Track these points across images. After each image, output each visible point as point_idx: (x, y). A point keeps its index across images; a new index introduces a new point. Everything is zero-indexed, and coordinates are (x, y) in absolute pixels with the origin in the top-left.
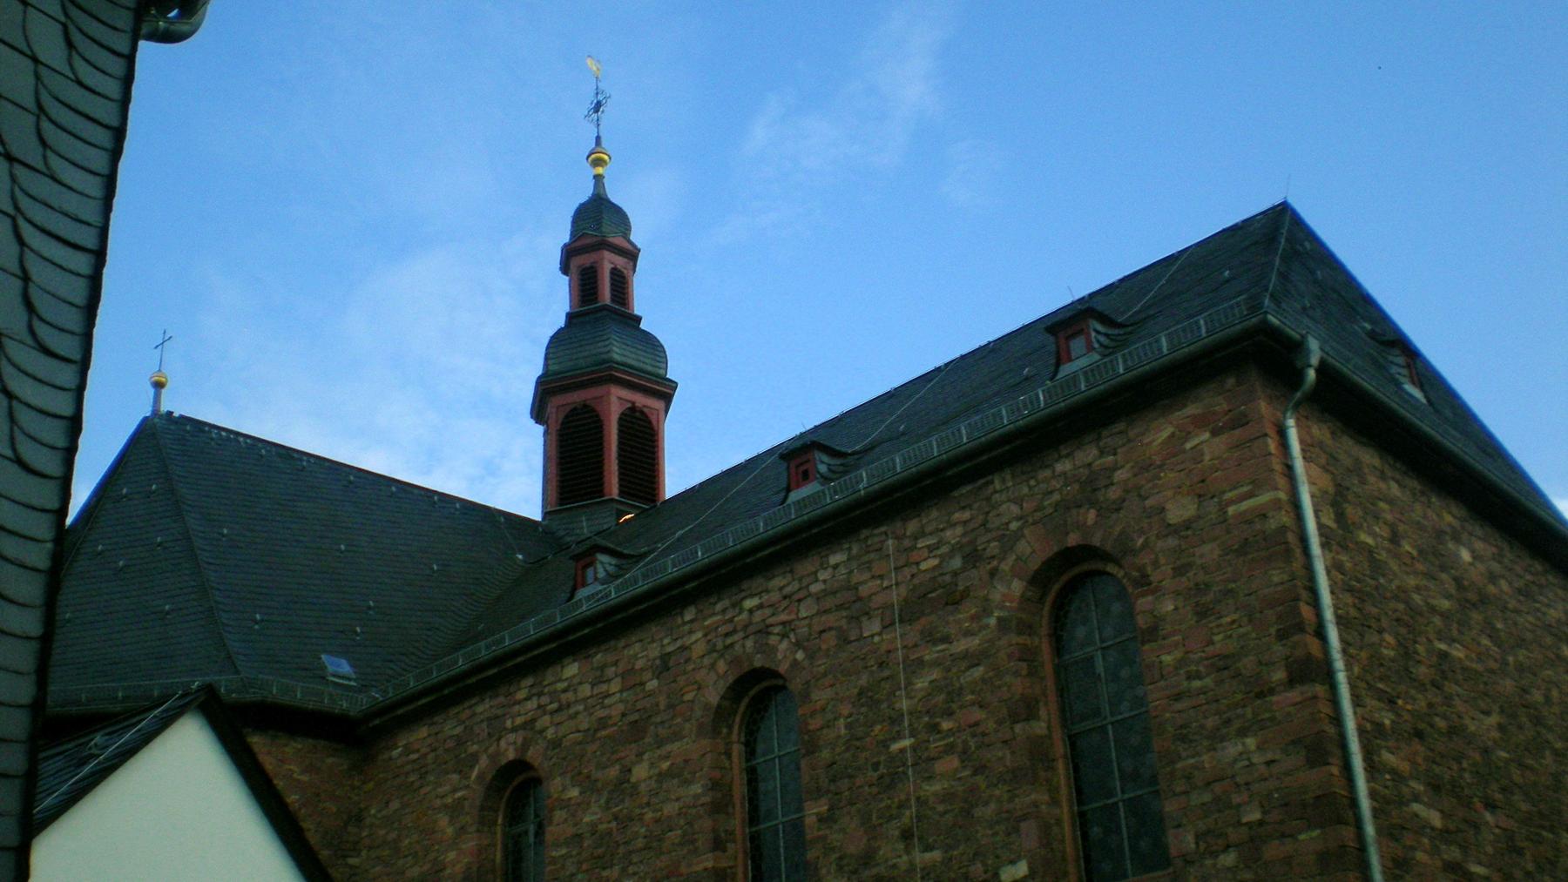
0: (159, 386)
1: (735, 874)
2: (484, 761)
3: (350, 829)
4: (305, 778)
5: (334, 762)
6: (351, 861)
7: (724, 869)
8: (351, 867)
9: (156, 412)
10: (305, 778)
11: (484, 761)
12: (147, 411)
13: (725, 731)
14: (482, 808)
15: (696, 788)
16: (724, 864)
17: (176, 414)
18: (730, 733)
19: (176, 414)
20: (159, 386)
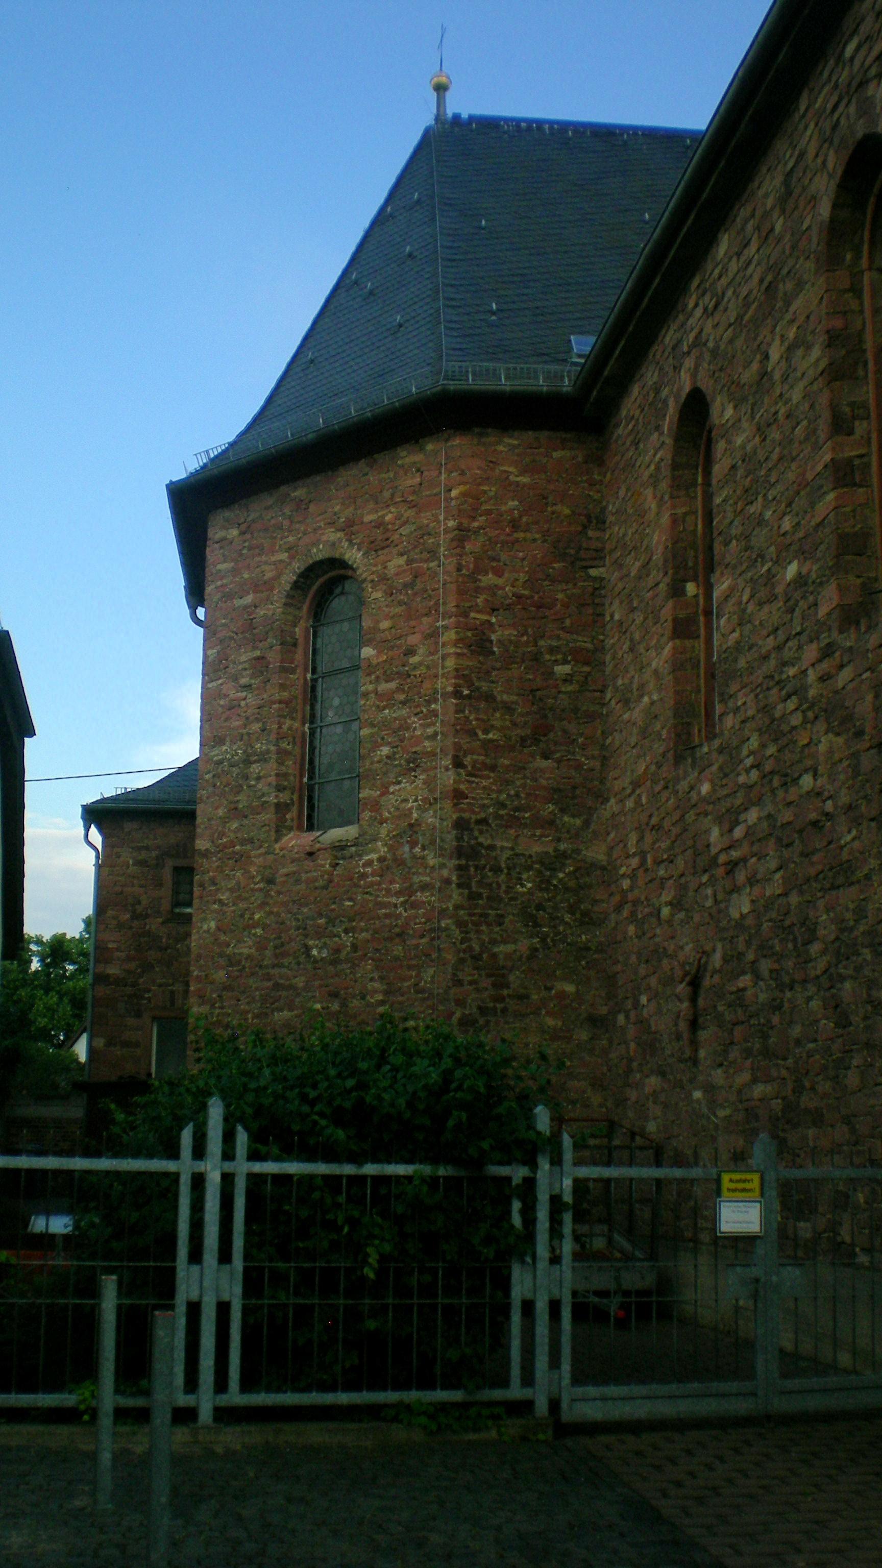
0: (440, 89)
1: (868, 465)
2: (671, 402)
3: (590, 533)
4: (525, 480)
5: (563, 454)
6: (593, 572)
7: (850, 461)
8: (595, 579)
9: (439, 117)
10: (525, 480)
11: (671, 402)
12: (427, 119)
13: (849, 257)
14: (675, 466)
15: (816, 352)
16: (850, 453)
17: (465, 115)
18: (858, 257)
19: (465, 115)
20: (440, 89)
